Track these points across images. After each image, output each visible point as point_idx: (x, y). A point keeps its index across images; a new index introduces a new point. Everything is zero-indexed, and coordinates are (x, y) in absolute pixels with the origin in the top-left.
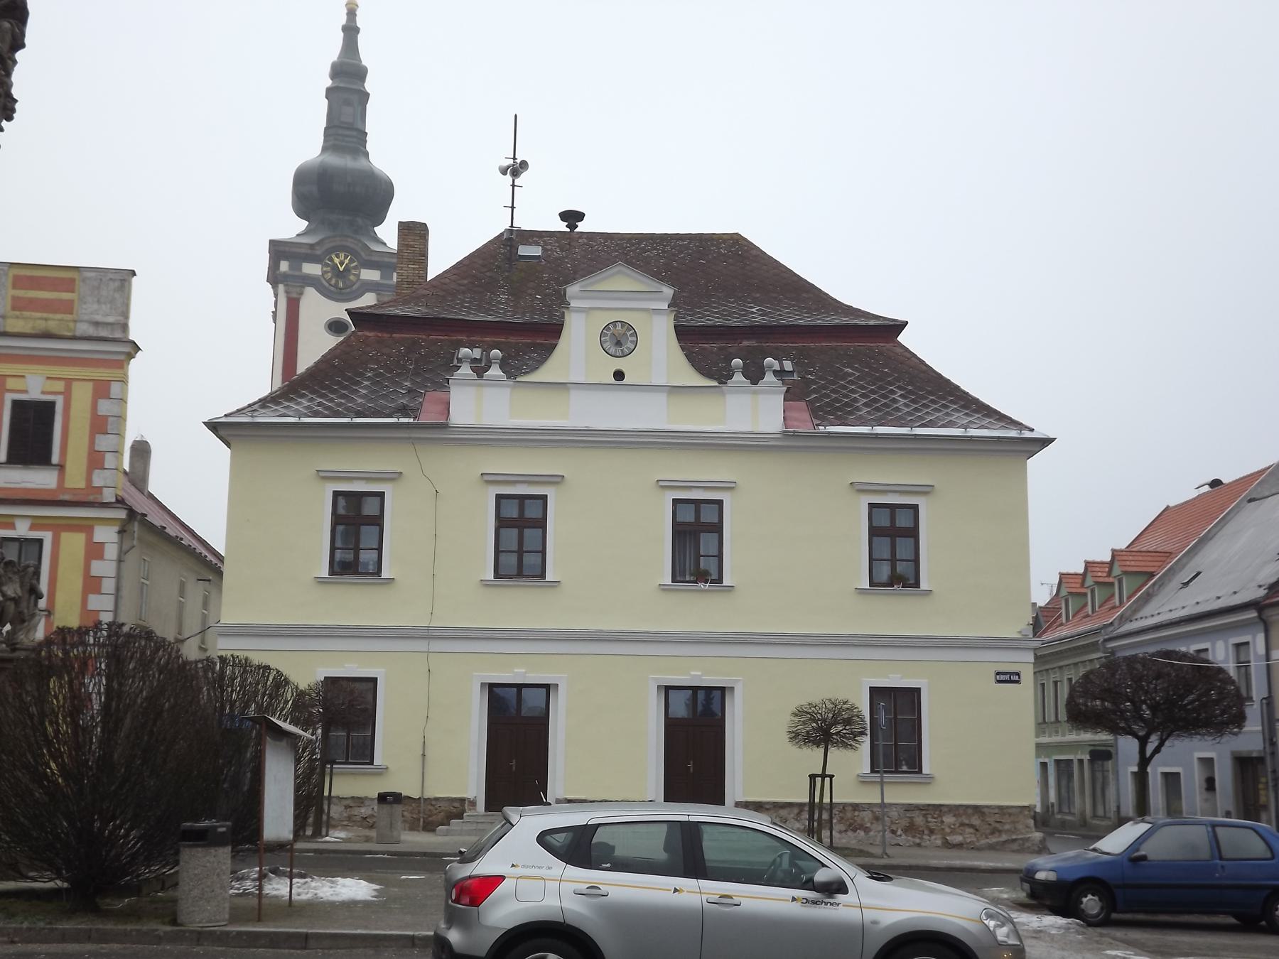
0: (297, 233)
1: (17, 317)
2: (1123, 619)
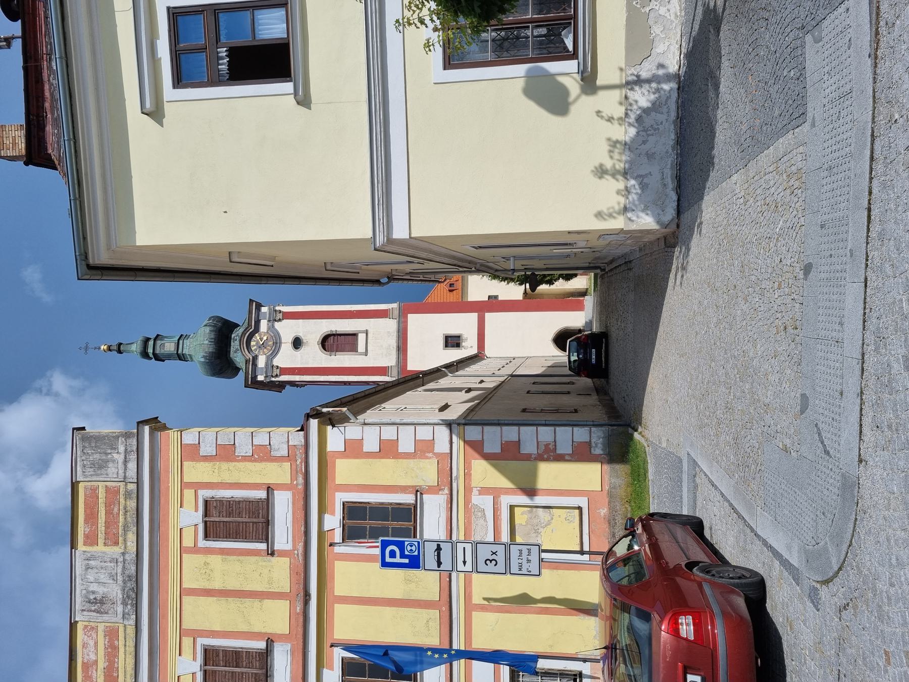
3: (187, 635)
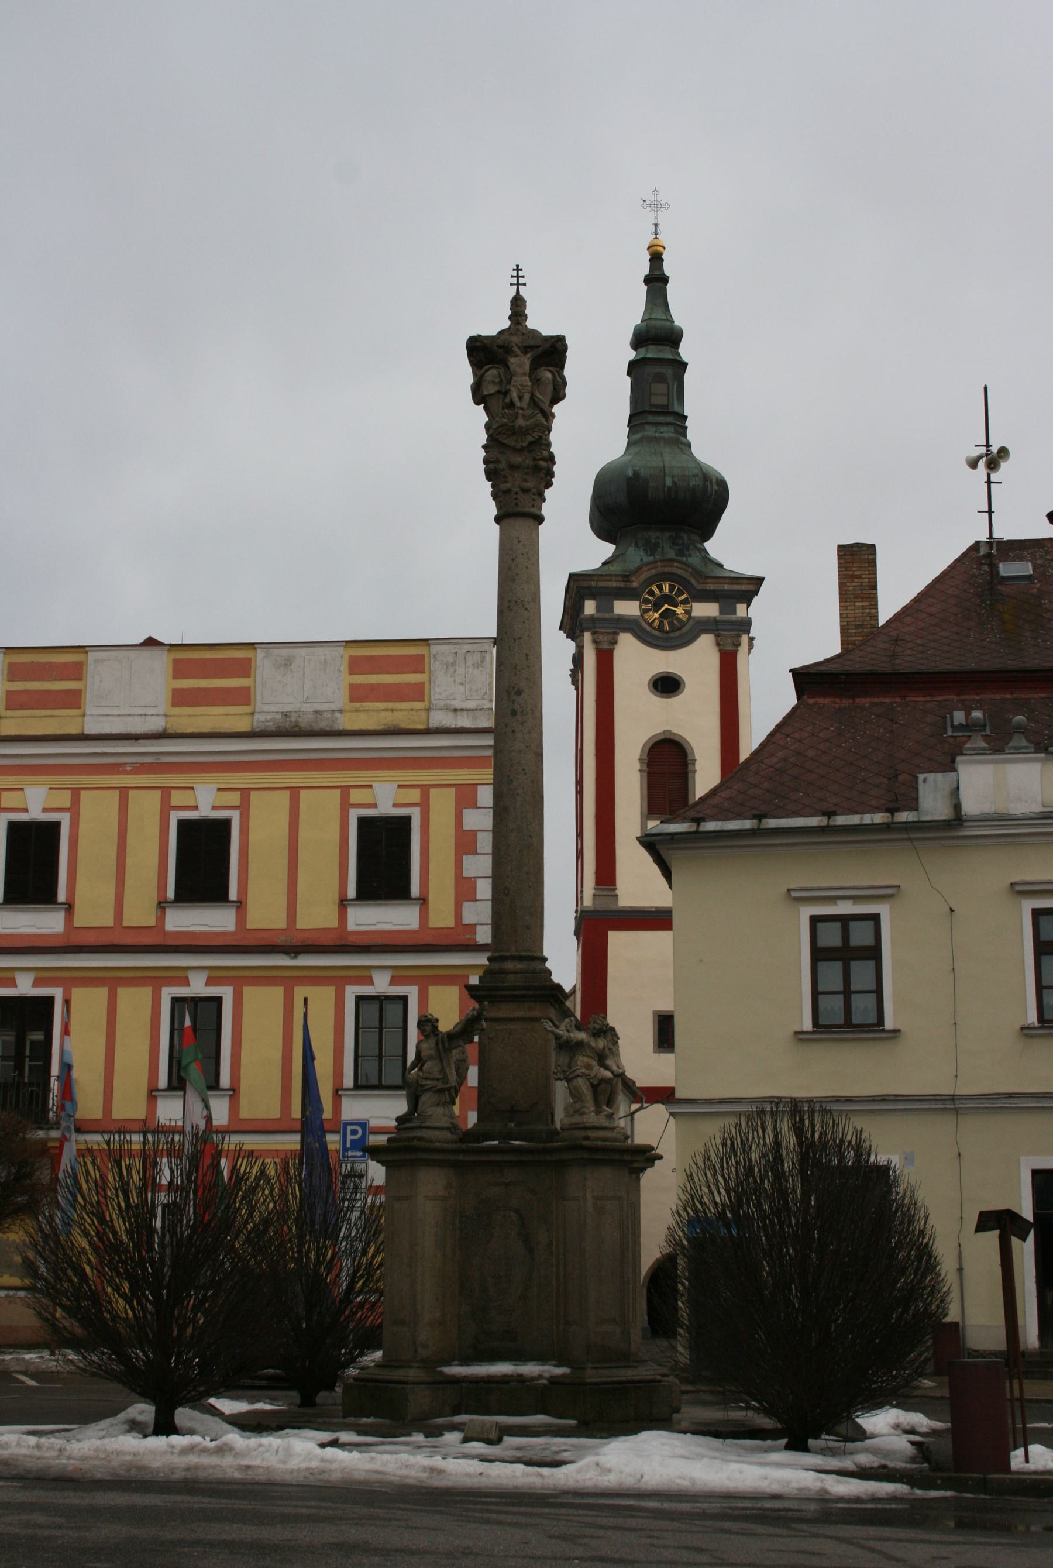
0: (603, 559)
1: (357, 710)
3: (242, 799)
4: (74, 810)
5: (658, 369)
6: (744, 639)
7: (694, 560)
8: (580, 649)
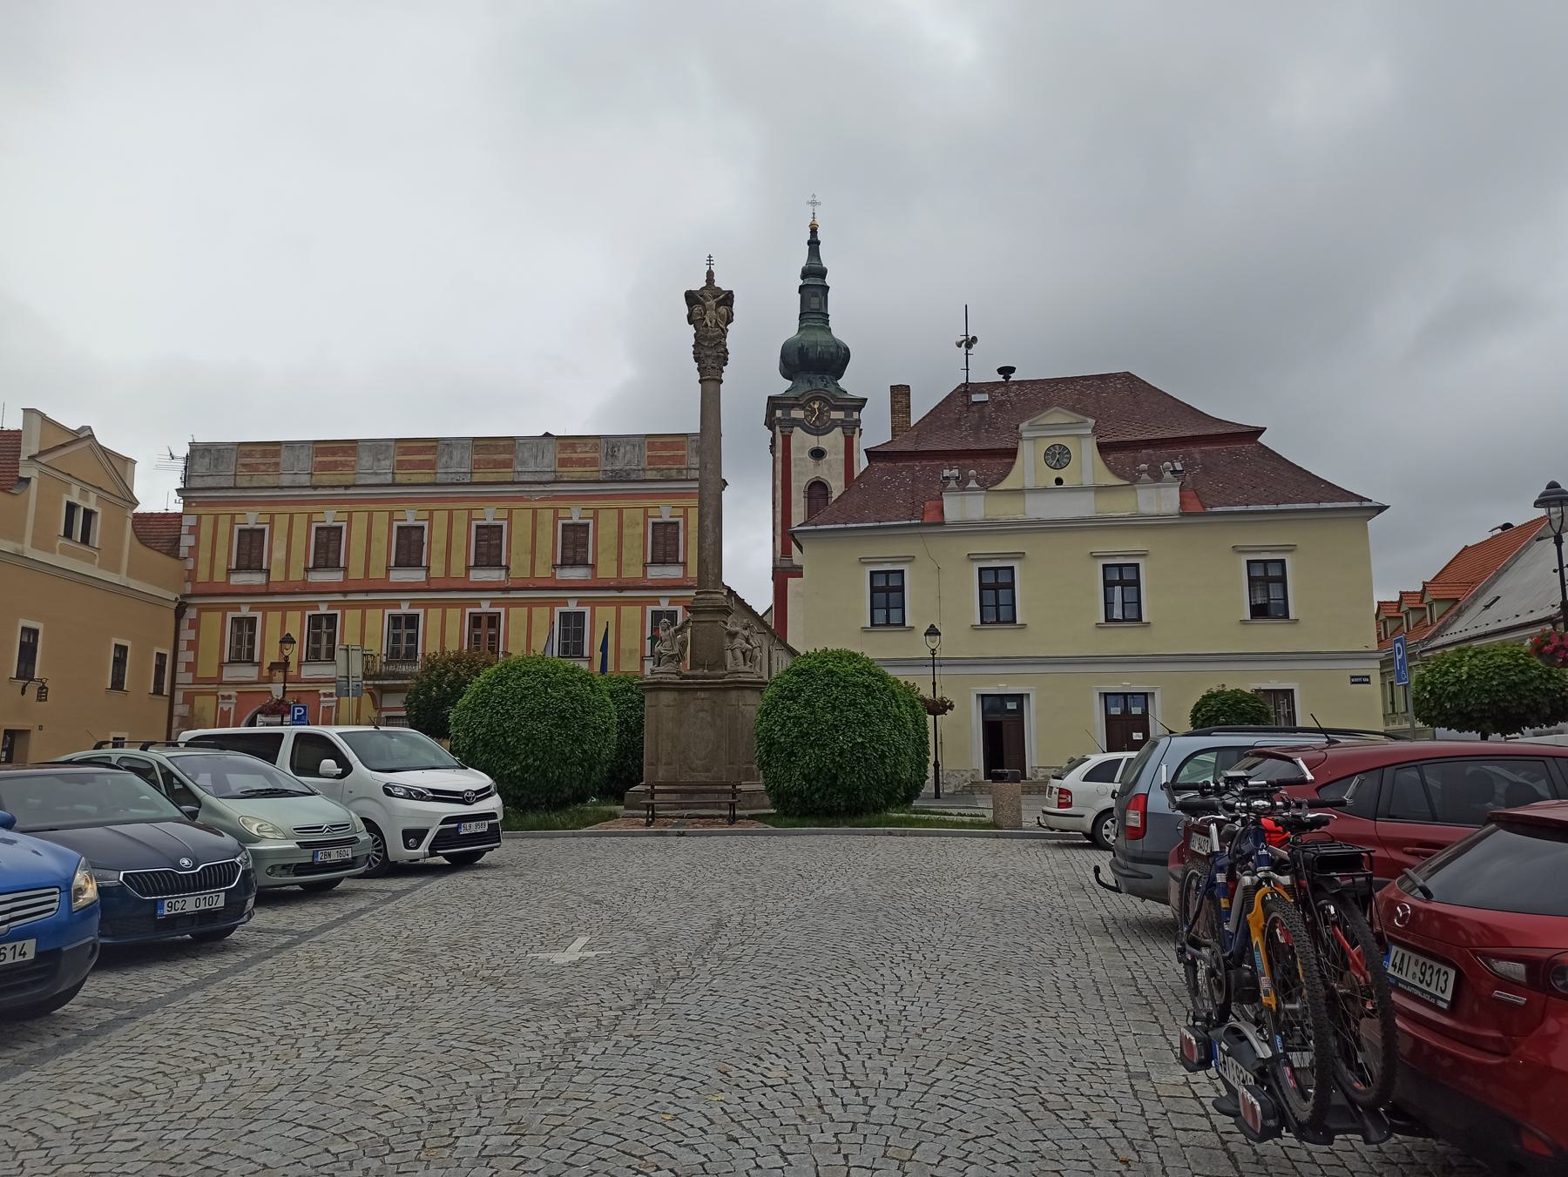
2: (1433, 637)
4: (509, 519)
5: (814, 290)
6: (857, 429)
7: (832, 389)
8: (774, 434)
